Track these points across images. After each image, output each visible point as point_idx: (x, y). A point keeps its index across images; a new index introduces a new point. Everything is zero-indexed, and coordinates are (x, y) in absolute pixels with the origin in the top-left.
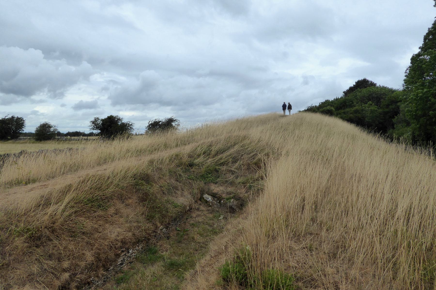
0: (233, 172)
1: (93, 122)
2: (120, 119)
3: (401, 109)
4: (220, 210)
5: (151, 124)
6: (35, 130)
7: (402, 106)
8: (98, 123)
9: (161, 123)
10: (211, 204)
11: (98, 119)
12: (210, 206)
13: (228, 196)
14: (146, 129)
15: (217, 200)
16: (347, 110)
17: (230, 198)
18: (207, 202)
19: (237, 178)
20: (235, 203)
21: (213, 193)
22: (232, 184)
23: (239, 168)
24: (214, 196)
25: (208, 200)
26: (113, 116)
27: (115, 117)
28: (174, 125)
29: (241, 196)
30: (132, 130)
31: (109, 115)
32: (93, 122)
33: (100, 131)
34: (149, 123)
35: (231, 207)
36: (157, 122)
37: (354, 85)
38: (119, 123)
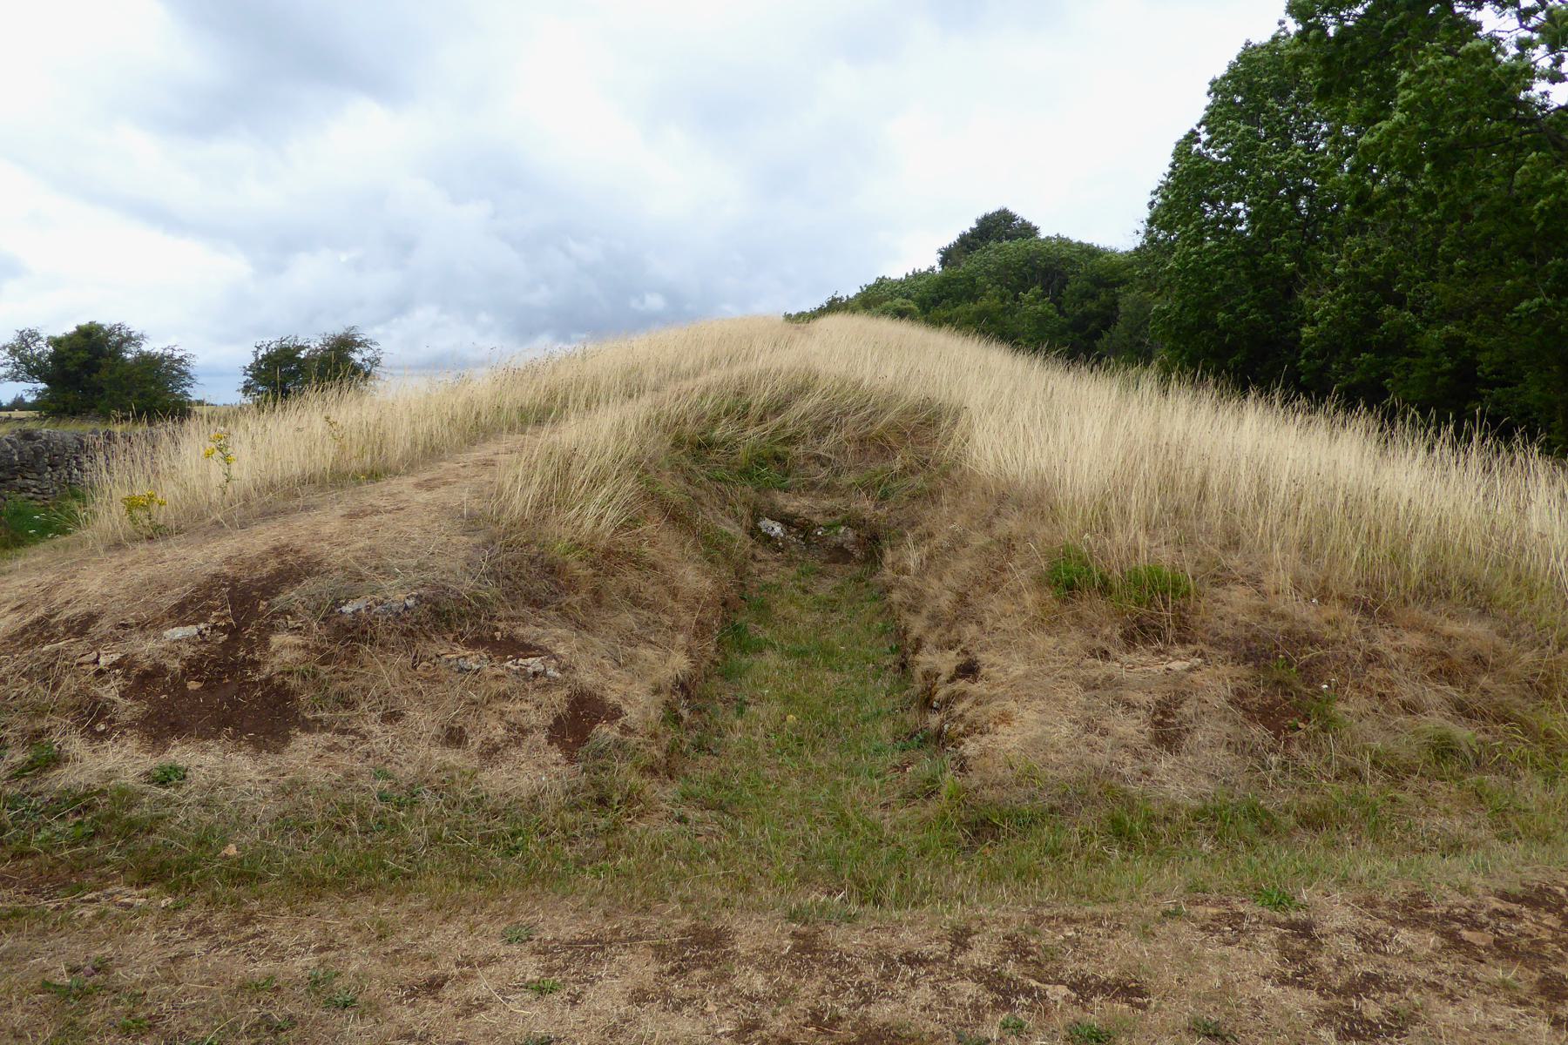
1: (13, 351)
2: (132, 339)
4: (808, 557)
5: (266, 358)
6: (1052, 234)
8: (36, 352)
9: (303, 354)
10: (780, 544)
11: (34, 335)
12: (780, 550)
13: (829, 520)
14: (246, 378)
15: (798, 532)
18: (769, 539)
19: (837, 474)
20: (851, 535)
21: (786, 515)
22: (829, 489)
23: (840, 450)
24: (787, 521)
25: (773, 534)
26: (100, 327)
27: (111, 332)
28: (360, 362)
29: (867, 516)
31: (84, 322)
32: (13, 351)
33: (42, 386)
34: (256, 354)
36: (287, 349)
37: (971, 229)
38: (129, 356)
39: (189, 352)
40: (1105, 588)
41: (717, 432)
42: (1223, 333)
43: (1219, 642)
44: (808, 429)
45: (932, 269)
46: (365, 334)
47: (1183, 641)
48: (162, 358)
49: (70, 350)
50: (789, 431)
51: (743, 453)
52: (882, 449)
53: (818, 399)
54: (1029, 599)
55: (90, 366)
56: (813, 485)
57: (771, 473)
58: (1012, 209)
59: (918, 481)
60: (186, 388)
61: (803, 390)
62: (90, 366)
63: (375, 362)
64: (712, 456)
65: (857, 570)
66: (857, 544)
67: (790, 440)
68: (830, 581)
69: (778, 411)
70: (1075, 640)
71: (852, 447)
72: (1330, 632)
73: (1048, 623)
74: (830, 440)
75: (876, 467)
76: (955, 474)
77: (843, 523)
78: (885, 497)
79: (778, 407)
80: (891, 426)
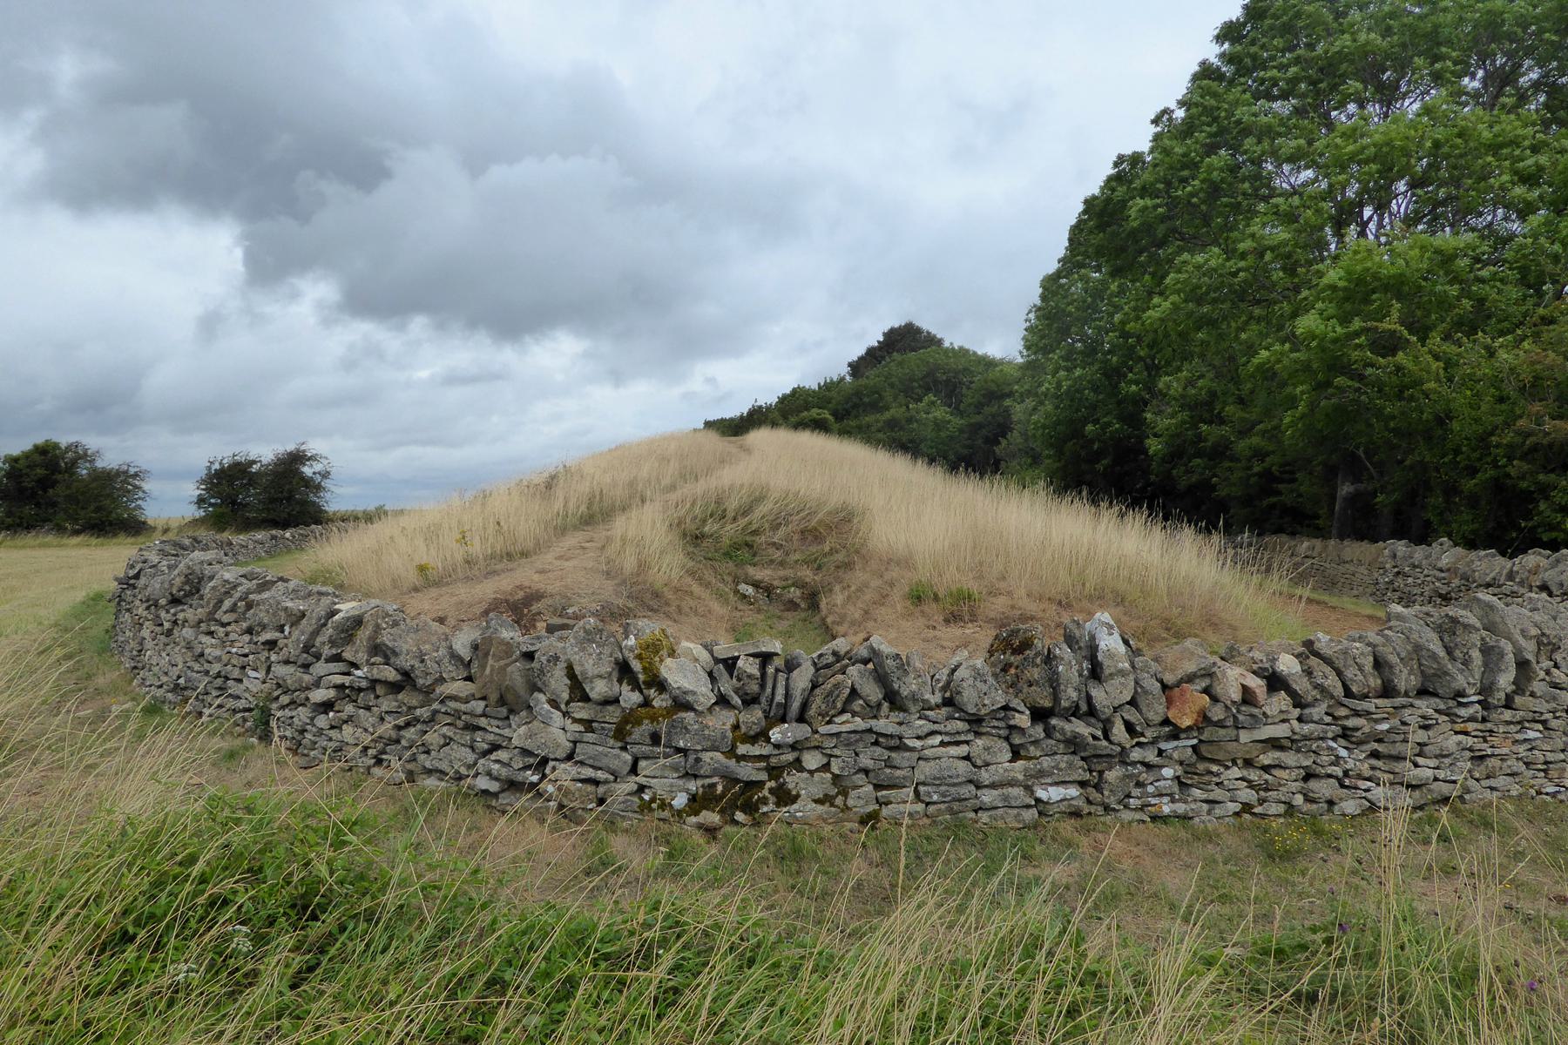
0: (777, 546)
3: (1015, 418)
7: (1018, 410)
14: (199, 492)
16: (869, 419)
17: (789, 586)
19: (787, 554)
20: (798, 593)
22: (782, 564)
23: (788, 539)
26: (56, 446)
29: (808, 580)
30: (141, 494)
35: (791, 601)
38: (85, 472)
39: (144, 467)
40: (936, 598)
41: (706, 529)
42: (1092, 441)
43: (990, 621)
44: (767, 525)
45: (842, 379)
46: (313, 446)
47: (971, 621)
48: (118, 473)
49: (28, 467)
50: (754, 527)
51: (726, 541)
52: (816, 538)
53: (771, 506)
54: (899, 607)
55: (45, 483)
56: (772, 561)
57: (744, 554)
58: (918, 323)
59: (840, 557)
60: (139, 502)
61: (760, 499)
62: (45, 483)
63: (326, 475)
64: (705, 544)
65: (803, 615)
66: (802, 598)
67: (755, 533)
68: (786, 622)
69: (745, 513)
70: (921, 622)
71: (796, 537)
72: (1041, 614)
73: (908, 615)
74: (782, 532)
75: (813, 549)
76: (864, 551)
77: (793, 585)
78: (819, 568)
79: (746, 511)
80: (820, 522)
